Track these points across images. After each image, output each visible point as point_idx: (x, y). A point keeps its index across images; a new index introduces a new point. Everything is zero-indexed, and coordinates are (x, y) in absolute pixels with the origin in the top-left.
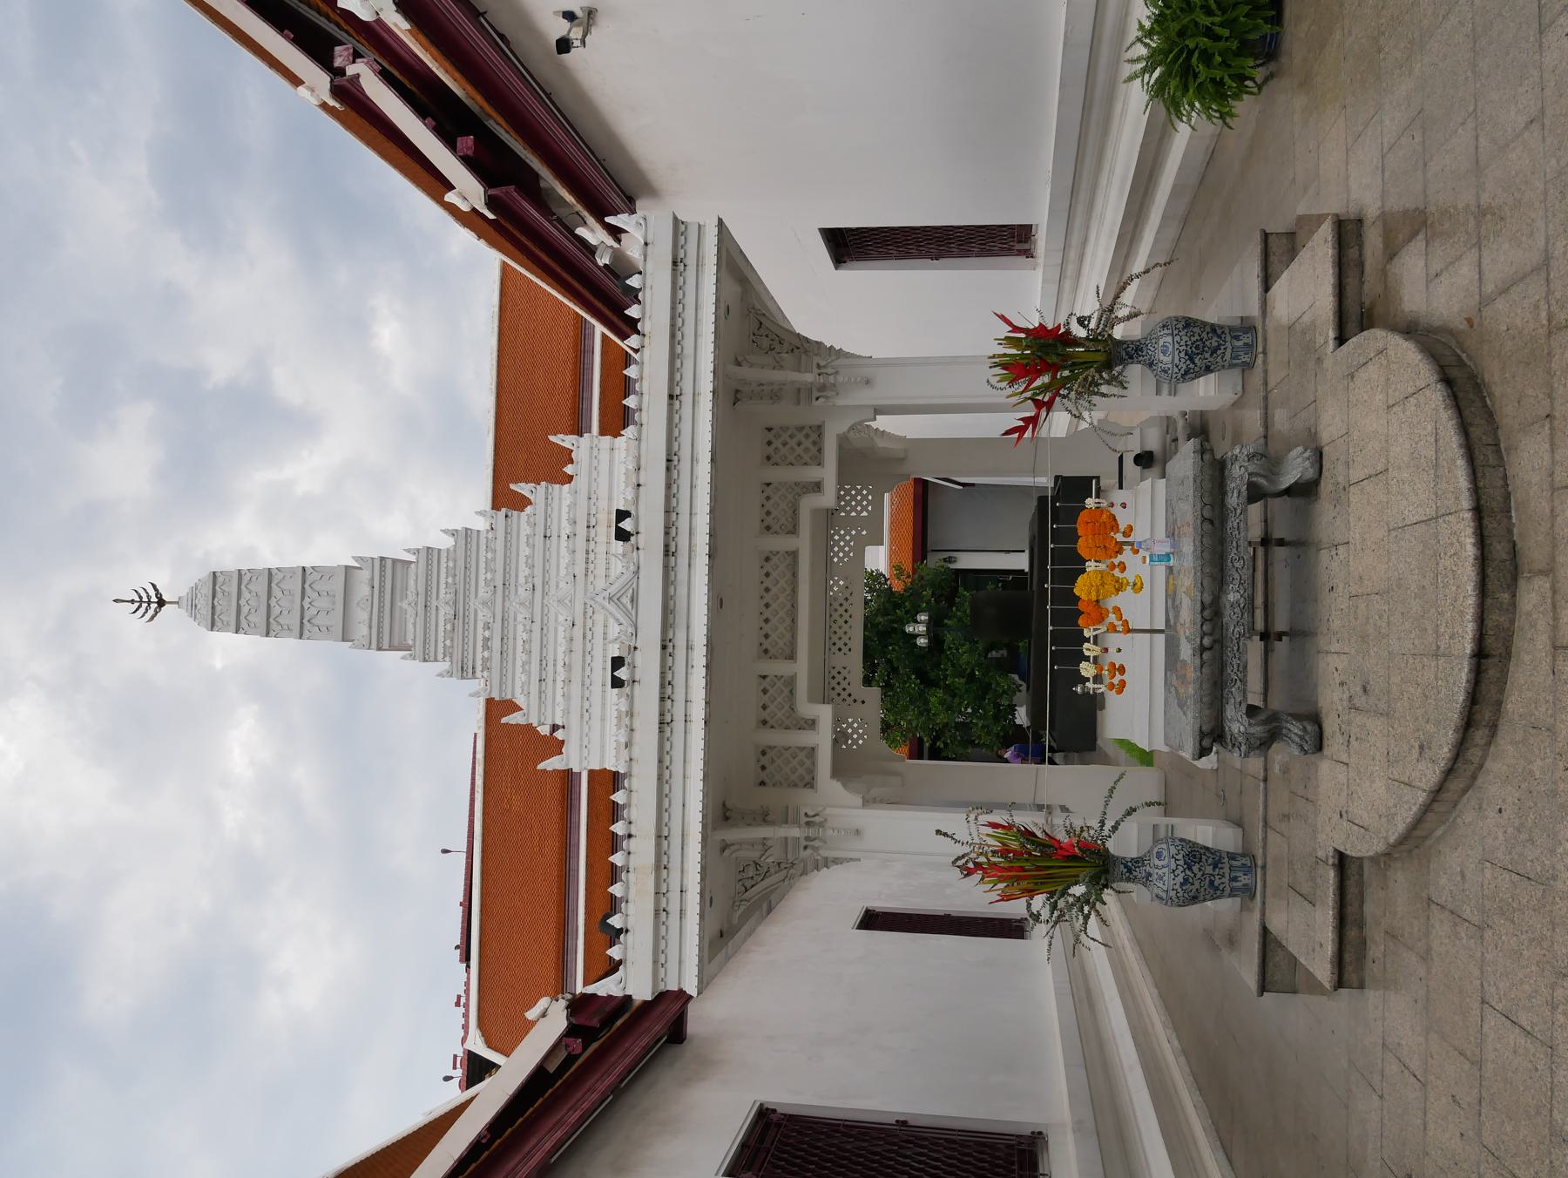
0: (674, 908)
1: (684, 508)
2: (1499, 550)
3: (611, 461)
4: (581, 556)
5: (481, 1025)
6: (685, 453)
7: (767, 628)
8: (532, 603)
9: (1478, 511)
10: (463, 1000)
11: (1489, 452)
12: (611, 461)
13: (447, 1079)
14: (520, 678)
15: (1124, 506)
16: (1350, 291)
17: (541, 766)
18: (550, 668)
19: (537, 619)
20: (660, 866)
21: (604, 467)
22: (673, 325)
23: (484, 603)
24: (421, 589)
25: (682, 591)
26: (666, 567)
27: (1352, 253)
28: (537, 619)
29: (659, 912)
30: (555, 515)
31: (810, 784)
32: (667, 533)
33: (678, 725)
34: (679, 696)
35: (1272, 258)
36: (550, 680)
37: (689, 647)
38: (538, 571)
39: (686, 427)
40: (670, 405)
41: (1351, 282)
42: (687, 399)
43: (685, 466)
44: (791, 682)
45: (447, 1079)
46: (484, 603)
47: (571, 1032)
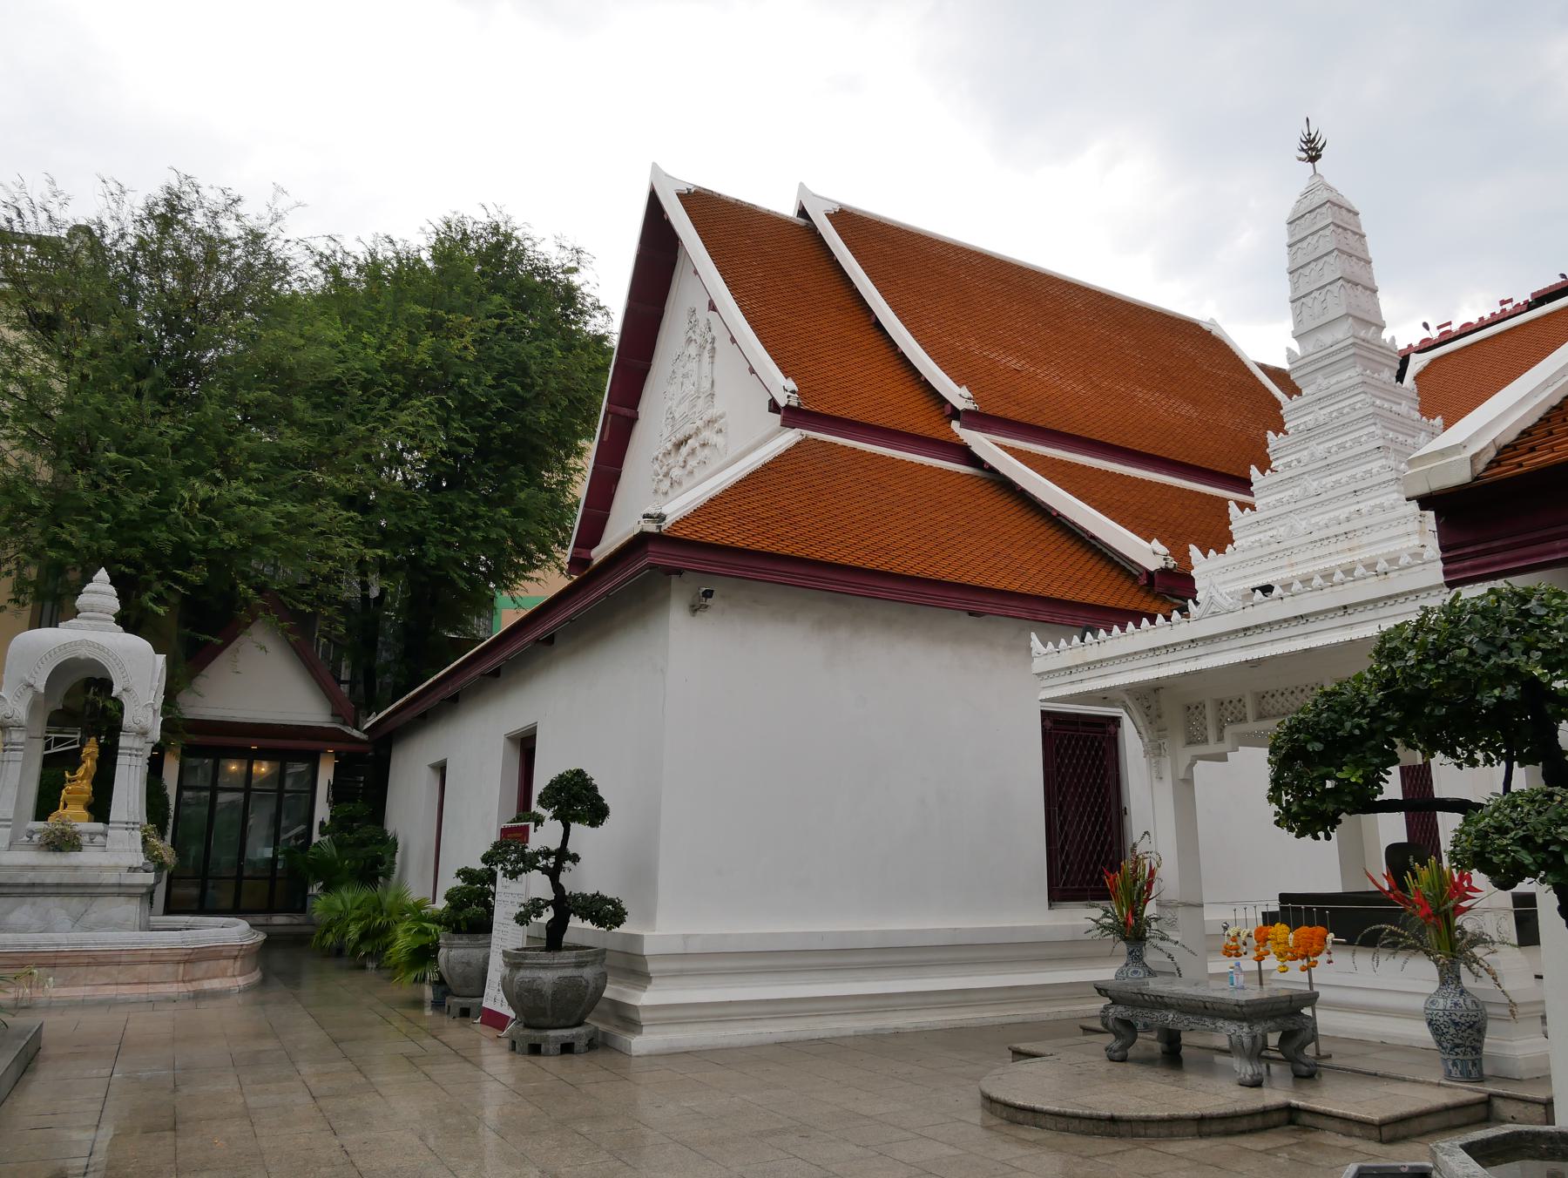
0: (1074, 677)
1: (1275, 635)
2: (1020, 1116)
3: (1399, 536)
4: (1323, 534)
5: (1434, 361)
6: (1310, 627)
7: (1307, 690)
8: (1308, 497)
9: (1033, 1110)
10: (1509, 307)
11: (1062, 1126)
12: (1399, 536)
13: (1426, 326)
14: (1271, 499)
15: (1330, 962)
16: (1330, 1123)
17: (1192, 547)
18: (1267, 527)
19: (1298, 505)
20: (1090, 665)
21: (1393, 532)
22: (1397, 595)
23: (1312, 454)
24: (1332, 390)
25: (1225, 645)
26: (1236, 631)
27: (1357, 1131)
28: (1298, 505)
29: (1069, 670)
30: (1373, 494)
31: (1190, 743)
32: (1256, 627)
33: (1156, 660)
34: (1171, 657)
35: (1522, 1105)
36: (1260, 529)
37: (1197, 658)
38: (1331, 494)
39: (1328, 624)
40: (1339, 608)
41: (1337, 1125)
42: (1347, 620)
43: (1301, 629)
44: (1243, 719)
45: (1426, 326)
46: (1312, 454)
47: (1149, 574)
